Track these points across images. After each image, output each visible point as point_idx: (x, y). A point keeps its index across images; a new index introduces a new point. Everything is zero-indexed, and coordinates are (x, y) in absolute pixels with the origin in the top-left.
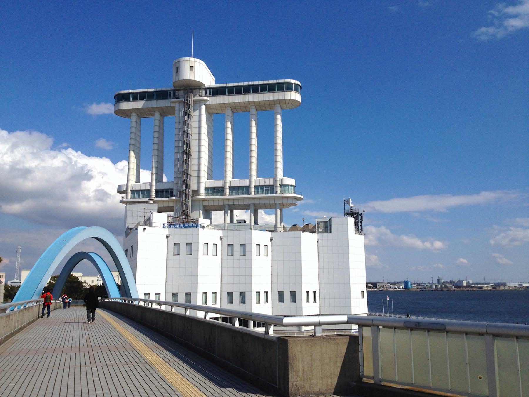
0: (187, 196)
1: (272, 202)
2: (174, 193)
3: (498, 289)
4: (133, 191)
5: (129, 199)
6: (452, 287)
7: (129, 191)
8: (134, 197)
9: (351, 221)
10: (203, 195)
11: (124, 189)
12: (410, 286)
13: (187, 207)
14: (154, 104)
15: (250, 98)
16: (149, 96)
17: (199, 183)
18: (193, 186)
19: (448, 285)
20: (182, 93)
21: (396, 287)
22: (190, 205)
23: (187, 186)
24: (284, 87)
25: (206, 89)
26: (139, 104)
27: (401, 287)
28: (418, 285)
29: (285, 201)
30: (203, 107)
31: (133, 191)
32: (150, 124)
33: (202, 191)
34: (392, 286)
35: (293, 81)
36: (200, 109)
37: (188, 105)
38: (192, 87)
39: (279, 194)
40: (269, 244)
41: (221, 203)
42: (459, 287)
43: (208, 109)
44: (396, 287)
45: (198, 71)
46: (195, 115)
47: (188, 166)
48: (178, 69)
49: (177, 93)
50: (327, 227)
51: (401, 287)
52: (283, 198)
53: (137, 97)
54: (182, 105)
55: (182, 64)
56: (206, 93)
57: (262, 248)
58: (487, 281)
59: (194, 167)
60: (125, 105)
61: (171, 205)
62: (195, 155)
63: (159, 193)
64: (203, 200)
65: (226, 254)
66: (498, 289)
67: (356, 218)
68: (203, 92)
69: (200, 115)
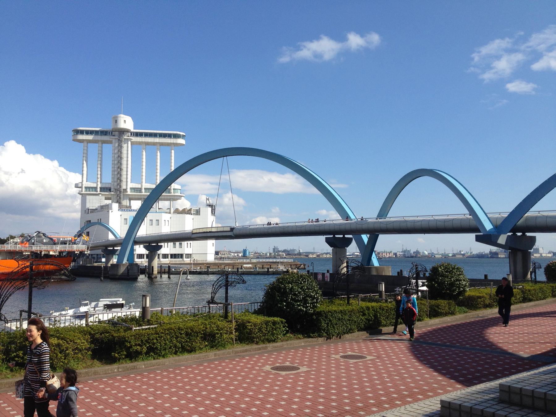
0: (120, 192)
1: (169, 198)
2: (112, 190)
3: (321, 257)
4: (86, 188)
5: (83, 192)
6: (283, 255)
7: (84, 187)
8: (86, 191)
9: (210, 209)
10: (129, 192)
11: (80, 185)
12: (248, 254)
13: (120, 198)
14: (99, 138)
15: (157, 140)
16: (96, 133)
17: (127, 185)
18: (124, 187)
19: (281, 253)
20: (117, 133)
21: (236, 255)
22: (122, 197)
23: (120, 187)
24: (176, 136)
25: (131, 133)
26: (90, 137)
27: (240, 255)
28: (255, 253)
29: (175, 198)
30: (130, 143)
31: (86, 188)
32: (93, 148)
33: (129, 190)
34: (233, 254)
35: (181, 133)
36: (128, 144)
37: (121, 141)
38: (123, 132)
39: (172, 194)
40: (169, 220)
41: (139, 197)
42: (289, 255)
43: (132, 143)
44: (236, 255)
45: (126, 122)
46: (125, 146)
47: (121, 175)
48: (116, 121)
49: (113, 133)
50: (198, 212)
51: (240, 255)
52: (175, 196)
53: (88, 133)
54: (117, 140)
55: (119, 119)
56: (131, 134)
57: (167, 222)
58: (315, 251)
59: (124, 176)
60: (80, 137)
61: (110, 196)
62: (125, 169)
63: (102, 189)
64: (129, 195)
65: (149, 224)
66: (321, 257)
67: (212, 208)
68: (130, 134)
69: (128, 147)
